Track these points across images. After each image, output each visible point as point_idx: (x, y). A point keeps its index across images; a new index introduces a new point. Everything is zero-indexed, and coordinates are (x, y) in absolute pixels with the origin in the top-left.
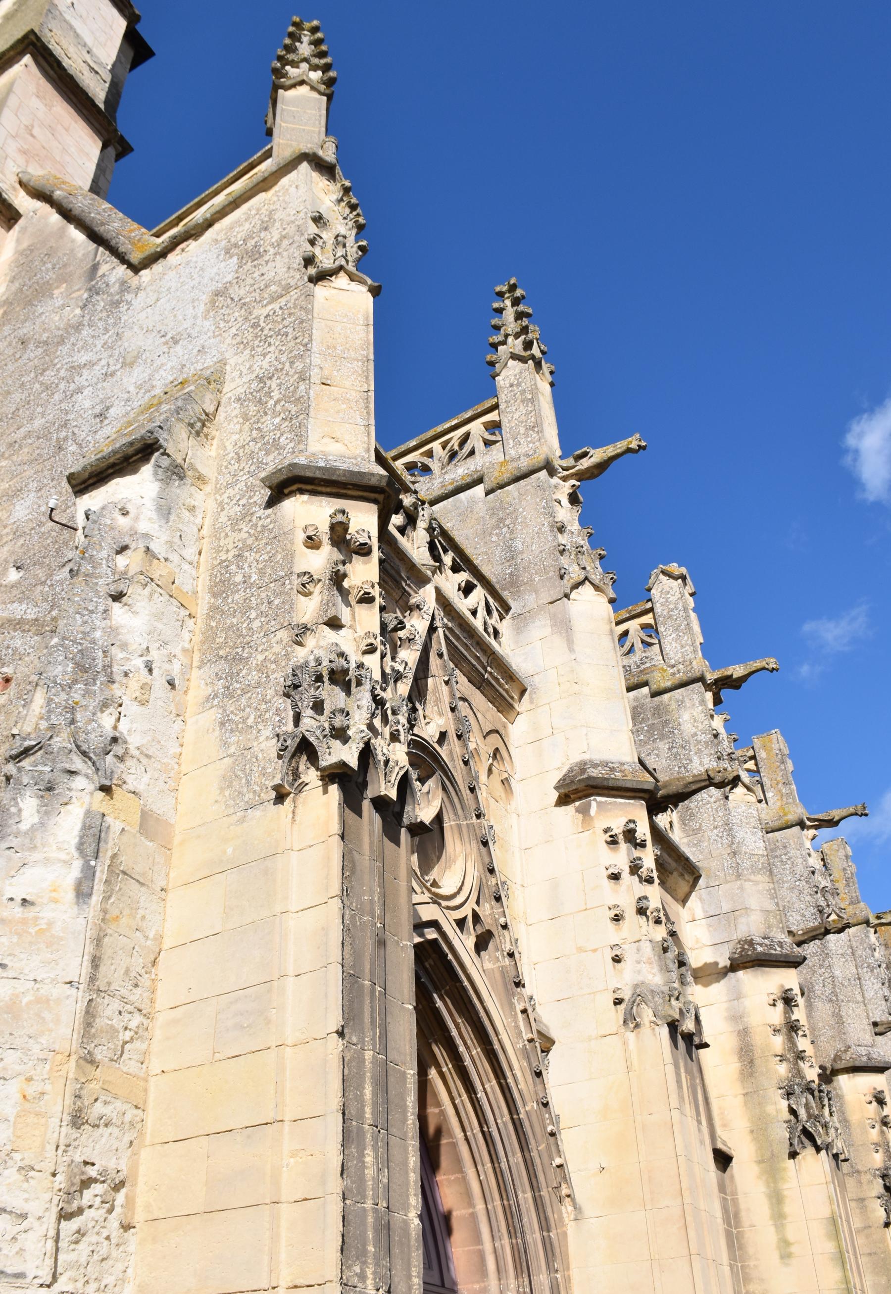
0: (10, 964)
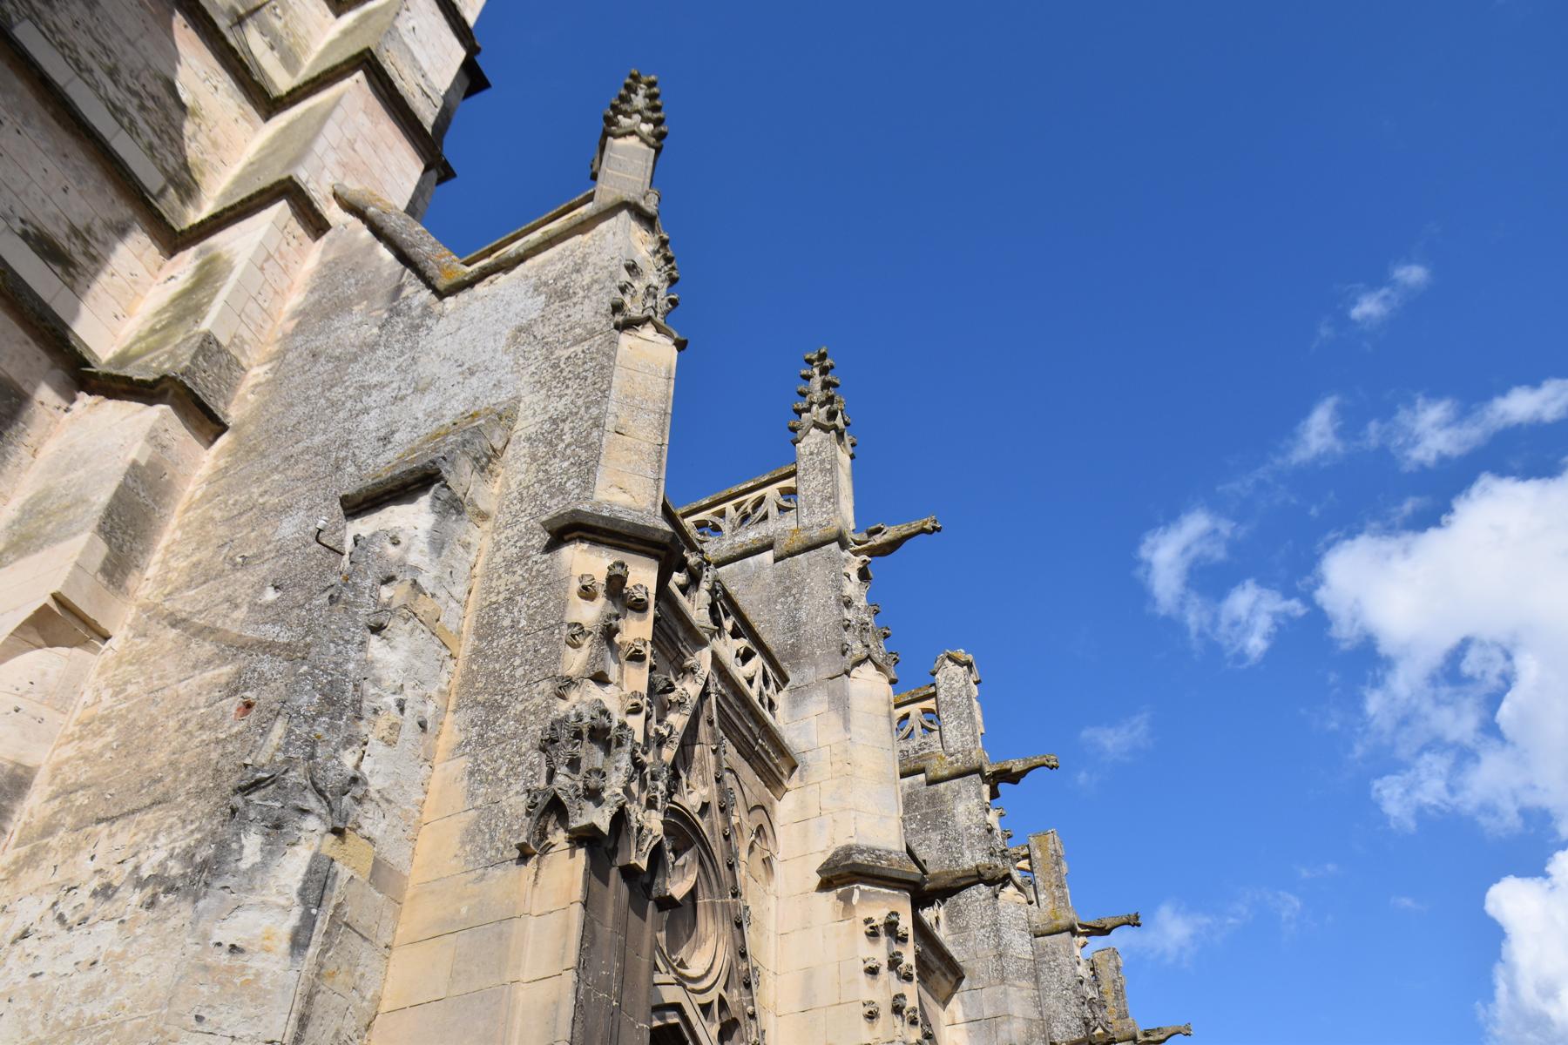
0: (207, 1017)
